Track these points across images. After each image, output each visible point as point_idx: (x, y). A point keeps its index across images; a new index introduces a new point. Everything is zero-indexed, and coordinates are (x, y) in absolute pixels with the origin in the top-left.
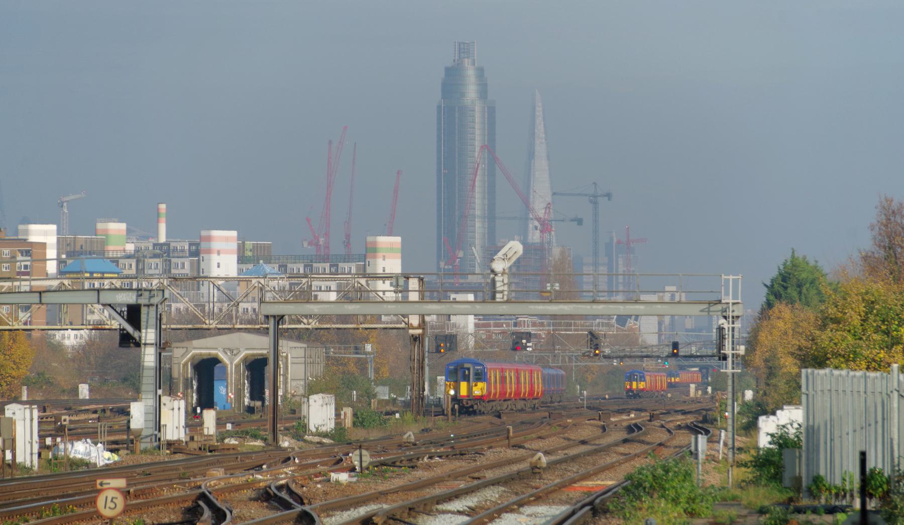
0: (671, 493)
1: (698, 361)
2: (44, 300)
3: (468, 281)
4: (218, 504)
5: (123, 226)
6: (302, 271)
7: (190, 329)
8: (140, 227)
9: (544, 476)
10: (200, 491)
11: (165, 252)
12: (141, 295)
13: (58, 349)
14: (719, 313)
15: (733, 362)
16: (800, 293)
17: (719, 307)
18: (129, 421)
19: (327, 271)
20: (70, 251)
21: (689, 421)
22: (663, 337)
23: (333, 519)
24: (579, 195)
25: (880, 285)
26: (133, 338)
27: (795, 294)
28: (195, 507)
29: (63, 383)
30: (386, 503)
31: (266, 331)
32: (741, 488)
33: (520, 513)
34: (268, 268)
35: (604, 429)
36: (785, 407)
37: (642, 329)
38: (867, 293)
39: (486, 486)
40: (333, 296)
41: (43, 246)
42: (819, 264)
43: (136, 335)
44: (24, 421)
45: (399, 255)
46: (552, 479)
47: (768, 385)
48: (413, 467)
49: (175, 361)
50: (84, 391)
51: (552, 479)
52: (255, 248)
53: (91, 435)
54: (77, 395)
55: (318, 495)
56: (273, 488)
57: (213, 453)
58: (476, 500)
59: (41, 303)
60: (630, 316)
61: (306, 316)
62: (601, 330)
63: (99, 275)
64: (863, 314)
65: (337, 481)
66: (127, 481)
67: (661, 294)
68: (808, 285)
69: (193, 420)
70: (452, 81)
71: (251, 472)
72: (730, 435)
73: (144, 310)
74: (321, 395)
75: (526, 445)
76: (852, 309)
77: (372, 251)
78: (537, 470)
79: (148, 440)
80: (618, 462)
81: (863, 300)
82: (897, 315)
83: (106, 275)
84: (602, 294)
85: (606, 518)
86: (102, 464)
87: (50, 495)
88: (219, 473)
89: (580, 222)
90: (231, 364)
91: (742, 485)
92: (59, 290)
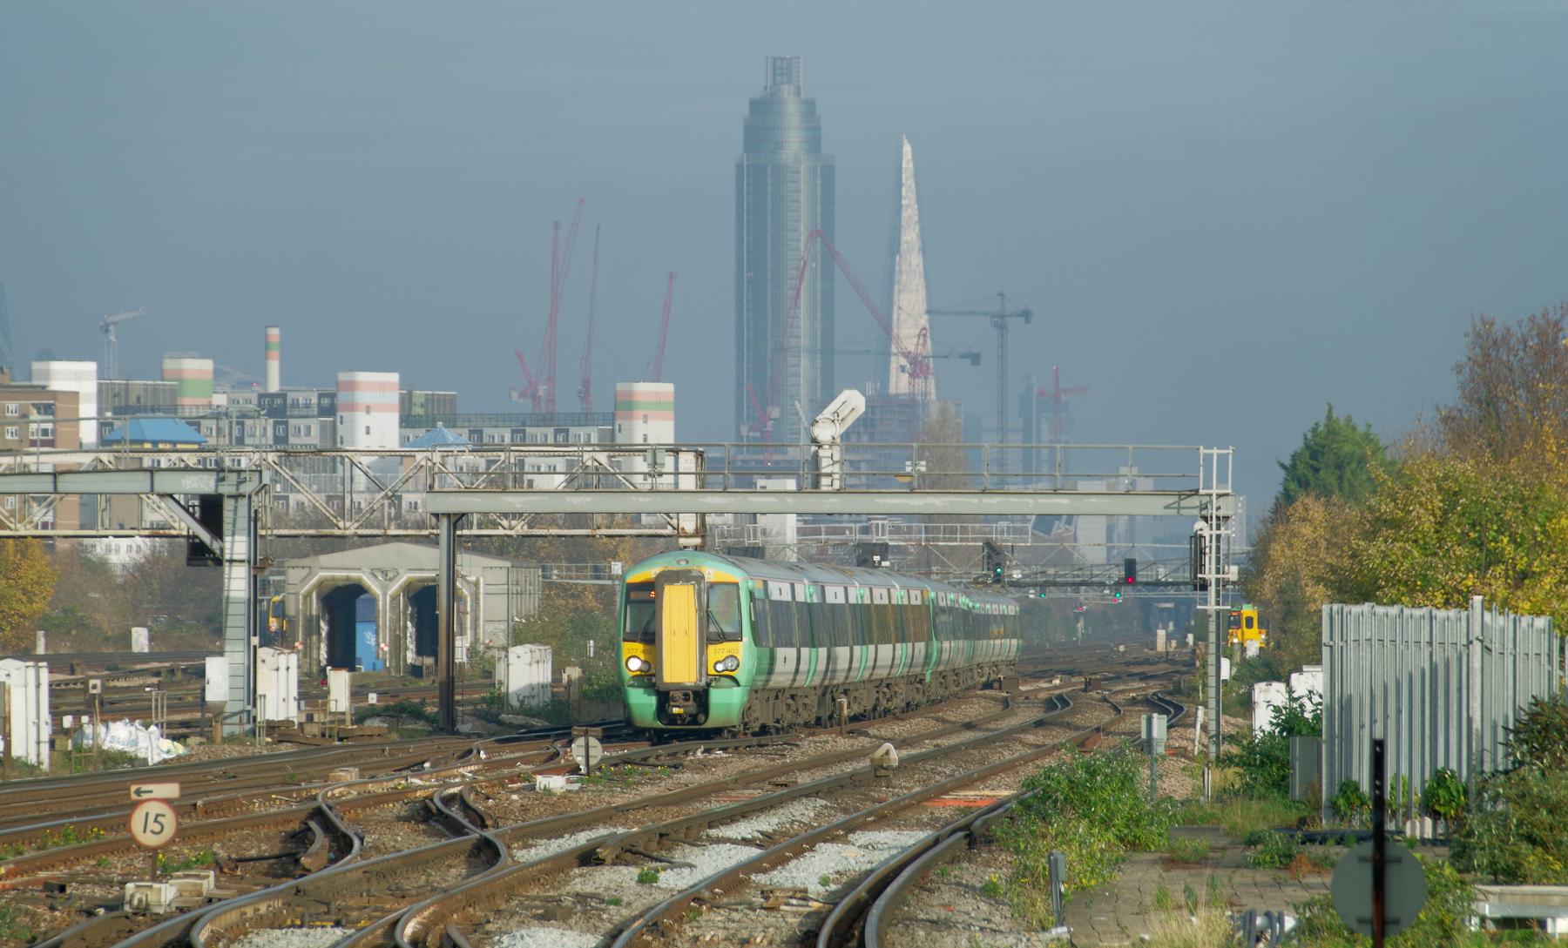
0: (1101, 811)
1: (1171, 592)
2: (61, 487)
3: (788, 457)
4: (343, 826)
5: (207, 365)
6: (507, 440)
7: (312, 536)
8: (237, 364)
9: (895, 782)
10: (314, 805)
11: (276, 408)
12: (223, 479)
13: (99, 568)
14: (1196, 512)
15: (1218, 592)
16: (1341, 479)
17: (1195, 501)
18: (204, 690)
19: (550, 440)
20: (119, 404)
21: (1151, 691)
22: (1115, 552)
23: (533, 851)
24: (972, 313)
25: (1469, 465)
26: (211, 552)
27: (1332, 480)
28: (302, 831)
29: (105, 626)
30: (624, 825)
31: (432, 541)
32: (1222, 801)
33: (847, 842)
34: (450, 435)
35: (1006, 703)
36: (1305, 668)
37: (1080, 538)
38: (1446, 478)
39: (794, 799)
40: (558, 481)
41: (74, 396)
42: (1373, 430)
43: (215, 546)
44: (26, 688)
45: (671, 414)
46: (908, 787)
47: (1284, 631)
48: (675, 767)
49: (291, 589)
50: (140, 639)
51: (908, 787)
52: (430, 400)
53: (138, 712)
54: (129, 645)
55: (512, 812)
56: (436, 800)
57: (345, 742)
58: (775, 820)
59: (56, 491)
60: (1058, 516)
61: (506, 515)
62: (1004, 540)
63: (168, 446)
64: (1439, 513)
65: (547, 791)
66: (182, 789)
67: (1113, 480)
68: (1354, 466)
69: (312, 689)
70: (761, 123)
71: (404, 773)
72: (1213, 714)
73: (228, 505)
74: (528, 647)
75: (871, 731)
76: (1421, 504)
77: (627, 406)
78: (883, 772)
79: (236, 719)
80: (1021, 758)
81: (1440, 489)
82: (1497, 514)
83: (179, 446)
84: (1015, 479)
85: (990, 852)
86: (157, 759)
87: (64, 810)
88: (350, 775)
89: (976, 359)
90: (385, 594)
91: (1224, 796)
92: (98, 470)
